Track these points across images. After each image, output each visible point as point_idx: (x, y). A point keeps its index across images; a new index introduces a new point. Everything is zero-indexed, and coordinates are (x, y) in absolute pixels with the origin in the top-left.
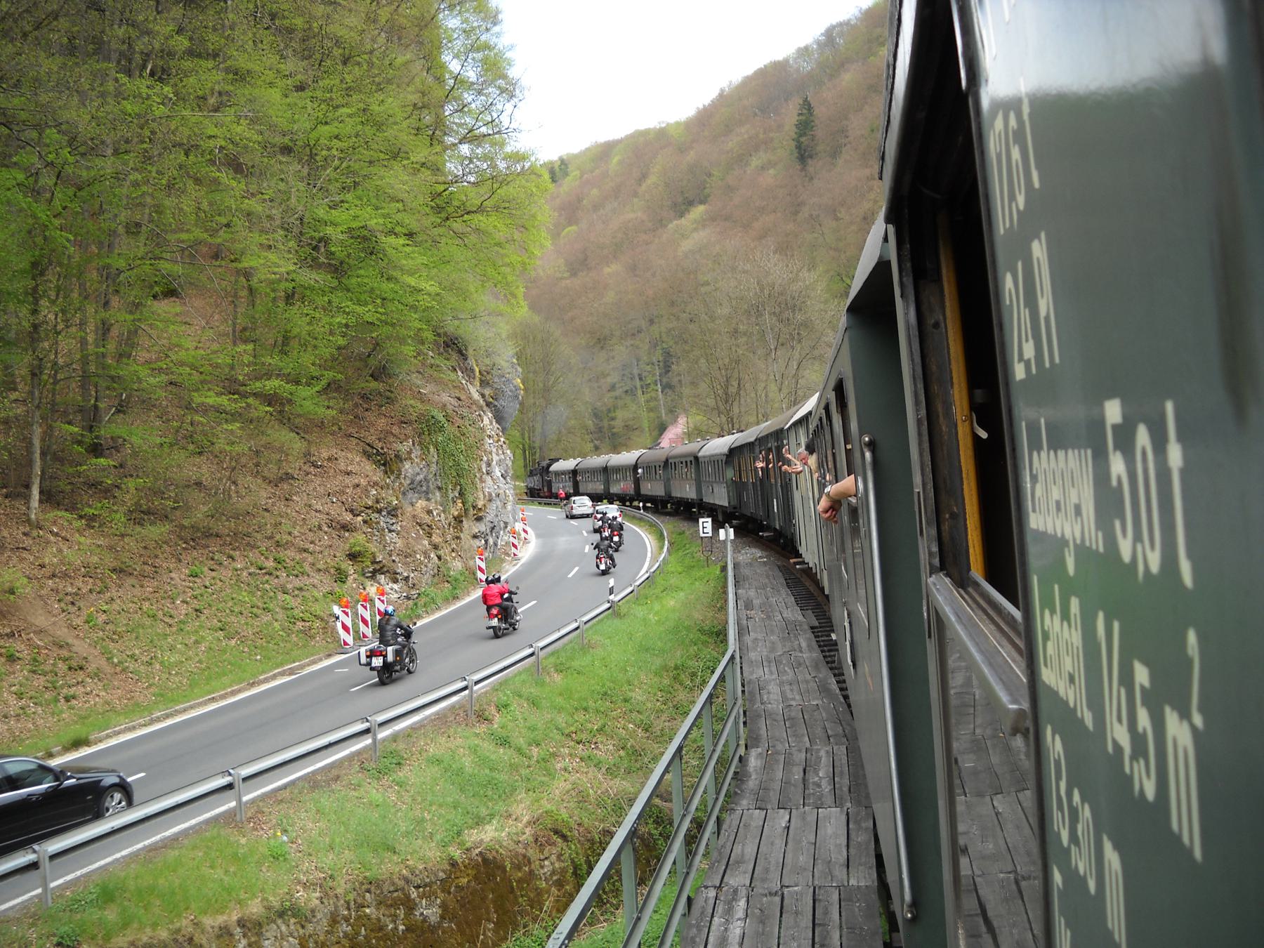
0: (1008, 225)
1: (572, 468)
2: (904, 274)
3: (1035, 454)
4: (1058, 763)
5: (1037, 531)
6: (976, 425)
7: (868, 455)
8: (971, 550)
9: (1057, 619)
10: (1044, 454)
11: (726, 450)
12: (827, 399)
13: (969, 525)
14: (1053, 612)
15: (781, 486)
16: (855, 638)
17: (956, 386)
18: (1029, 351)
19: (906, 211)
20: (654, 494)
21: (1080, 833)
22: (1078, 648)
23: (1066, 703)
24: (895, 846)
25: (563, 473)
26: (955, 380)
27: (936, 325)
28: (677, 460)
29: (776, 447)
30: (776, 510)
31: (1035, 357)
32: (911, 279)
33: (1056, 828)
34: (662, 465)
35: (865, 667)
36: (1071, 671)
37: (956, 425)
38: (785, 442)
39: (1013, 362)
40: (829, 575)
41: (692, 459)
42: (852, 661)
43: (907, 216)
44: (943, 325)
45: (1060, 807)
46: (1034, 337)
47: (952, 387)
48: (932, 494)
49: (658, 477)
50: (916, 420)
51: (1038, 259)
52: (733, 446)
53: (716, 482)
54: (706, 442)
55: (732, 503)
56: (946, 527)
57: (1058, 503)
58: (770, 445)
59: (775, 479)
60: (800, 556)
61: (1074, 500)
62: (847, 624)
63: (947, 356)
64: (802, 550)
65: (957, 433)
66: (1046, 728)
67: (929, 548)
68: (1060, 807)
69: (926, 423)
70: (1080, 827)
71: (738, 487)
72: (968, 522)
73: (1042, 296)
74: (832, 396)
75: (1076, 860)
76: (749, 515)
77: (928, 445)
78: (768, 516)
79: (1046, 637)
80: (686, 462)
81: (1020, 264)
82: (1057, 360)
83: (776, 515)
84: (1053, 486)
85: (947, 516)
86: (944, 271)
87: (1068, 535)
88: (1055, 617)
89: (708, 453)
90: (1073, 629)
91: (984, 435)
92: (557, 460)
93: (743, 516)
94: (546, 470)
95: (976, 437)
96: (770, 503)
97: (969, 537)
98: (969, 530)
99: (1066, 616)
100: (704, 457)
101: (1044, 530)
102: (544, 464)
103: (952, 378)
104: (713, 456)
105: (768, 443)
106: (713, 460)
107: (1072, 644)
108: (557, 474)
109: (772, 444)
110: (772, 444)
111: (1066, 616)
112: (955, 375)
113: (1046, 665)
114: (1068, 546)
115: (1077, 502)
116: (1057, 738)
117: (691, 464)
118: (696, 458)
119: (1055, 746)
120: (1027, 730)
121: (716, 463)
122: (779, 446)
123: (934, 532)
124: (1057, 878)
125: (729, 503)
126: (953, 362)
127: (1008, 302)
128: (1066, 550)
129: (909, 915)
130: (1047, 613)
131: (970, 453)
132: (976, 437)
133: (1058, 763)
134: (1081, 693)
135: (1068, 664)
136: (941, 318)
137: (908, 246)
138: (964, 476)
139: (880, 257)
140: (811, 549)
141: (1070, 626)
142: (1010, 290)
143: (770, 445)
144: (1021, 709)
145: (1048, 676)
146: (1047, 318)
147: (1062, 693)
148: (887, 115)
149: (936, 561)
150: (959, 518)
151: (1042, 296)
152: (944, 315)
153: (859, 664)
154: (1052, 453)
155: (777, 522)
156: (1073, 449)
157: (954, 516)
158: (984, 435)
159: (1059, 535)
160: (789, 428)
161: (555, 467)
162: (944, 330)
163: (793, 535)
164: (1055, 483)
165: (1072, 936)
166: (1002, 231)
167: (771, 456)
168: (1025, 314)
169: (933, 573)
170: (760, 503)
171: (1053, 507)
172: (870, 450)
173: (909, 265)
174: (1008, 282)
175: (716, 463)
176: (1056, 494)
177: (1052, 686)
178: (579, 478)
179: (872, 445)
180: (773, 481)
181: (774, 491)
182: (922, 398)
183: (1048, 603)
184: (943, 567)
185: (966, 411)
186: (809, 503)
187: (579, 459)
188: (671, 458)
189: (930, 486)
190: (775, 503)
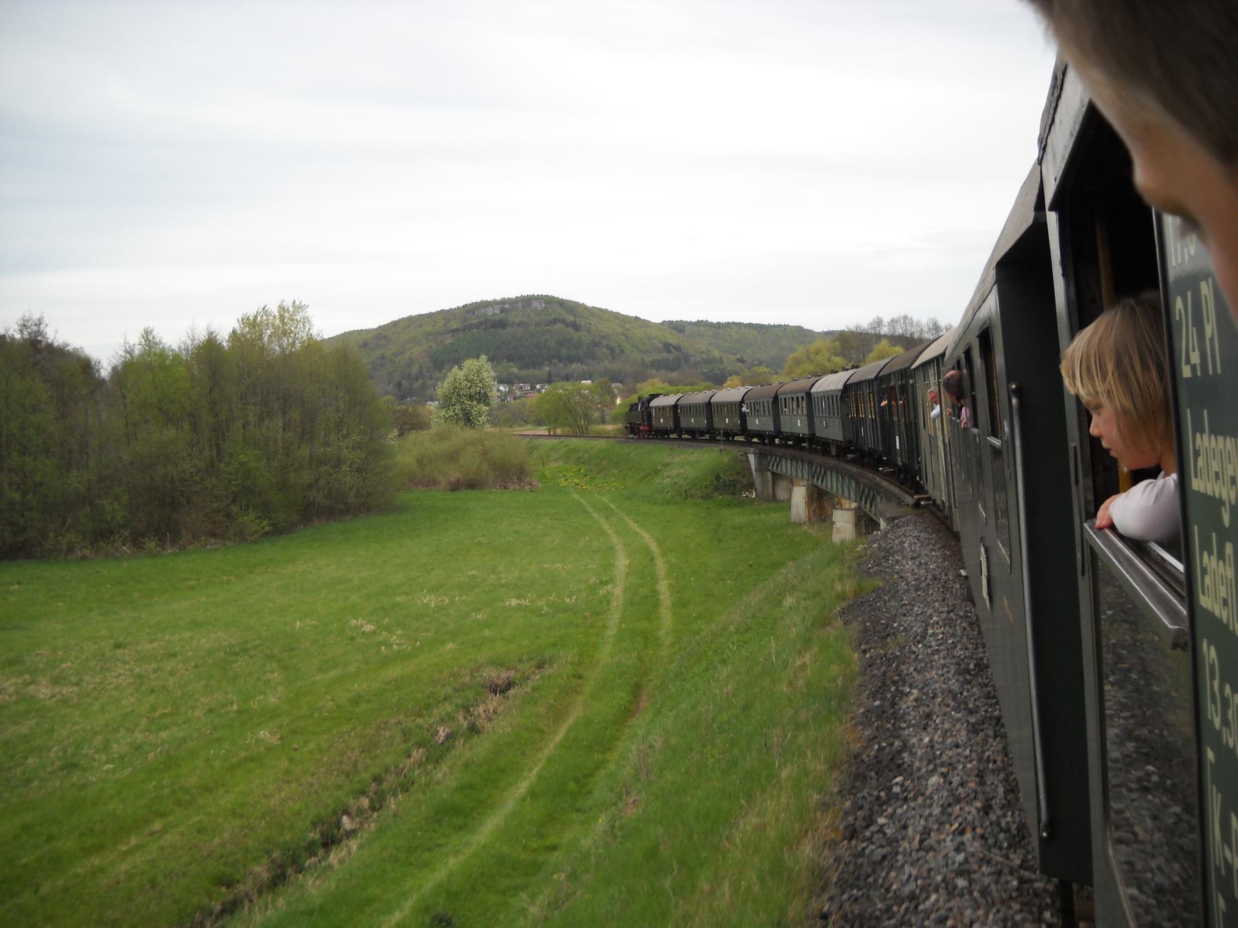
0: (1179, 262)
3: (1198, 436)
4: (1212, 667)
5: (1198, 493)
7: (1014, 401)
9: (1214, 558)
10: (1206, 436)
11: (841, 386)
14: (1210, 553)
16: (992, 574)
18: (1195, 358)
21: (1230, 717)
22: (1231, 580)
23: (1220, 621)
25: (663, 408)
28: (787, 396)
30: (898, 448)
31: (1201, 364)
33: (1210, 717)
36: (1225, 597)
39: (1180, 364)
41: (804, 395)
45: (1214, 701)
46: (1199, 349)
51: (1206, 296)
52: (849, 382)
57: (1217, 474)
60: (927, 492)
61: (1231, 473)
64: (929, 487)
66: (1203, 641)
68: (1214, 701)
70: (1230, 713)
73: (1208, 323)
75: (1227, 737)
79: (1204, 571)
80: (798, 398)
81: (1189, 293)
82: (1219, 371)
84: (1213, 462)
85: (1101, 468)
86: (1101, 254)
87: (1225, 497)
88: (1212, 557)
89: (821, 389)
90: (1227, 567)
92: (657, 396)
99: (1221, 556)
101: (1212, 495)
106: (828, 396)
107: (1226, 577)
111: (1221, 556)
113: (1204, 594)
114: (1224, 505)
115: (1233, 474)
116: (1213, 649)
118: (809, 394)
119: (1210, 654)
120: (1186, 644)
123: (1090, 482)
124: (1210, 755)
125: (844, 437)
127: (1177, 318)
128: (1223, 508)
129: (1045, 834)
130: (1205, 554)
134: (1233, 613)
135: (1223, 592)
141: (1225, 564)
142: (1180, 310)
145: (1205, 601)
146: (1212, 339)
147: (1217, 613)
148: (1051, 116)
151: (1208, 323)
152: (1100, 293)
153: (996, 598)
154: (1213, 437)
155: (899, 459)
156: (1231, 436)
159: (1217, 496)
161: (654, 403)
164: (1214, 459)
165: (1223, 799)
166: (1174, 265)
168: (1193, 331)
171: (1213, 476)
174: (1179, 304)
175: (830, 398)
176: (1215, 466)
177: (1209, 608)
179: (1019, 392)
180: (895, 419)
183: (1205, 545)
188: (781, 394)
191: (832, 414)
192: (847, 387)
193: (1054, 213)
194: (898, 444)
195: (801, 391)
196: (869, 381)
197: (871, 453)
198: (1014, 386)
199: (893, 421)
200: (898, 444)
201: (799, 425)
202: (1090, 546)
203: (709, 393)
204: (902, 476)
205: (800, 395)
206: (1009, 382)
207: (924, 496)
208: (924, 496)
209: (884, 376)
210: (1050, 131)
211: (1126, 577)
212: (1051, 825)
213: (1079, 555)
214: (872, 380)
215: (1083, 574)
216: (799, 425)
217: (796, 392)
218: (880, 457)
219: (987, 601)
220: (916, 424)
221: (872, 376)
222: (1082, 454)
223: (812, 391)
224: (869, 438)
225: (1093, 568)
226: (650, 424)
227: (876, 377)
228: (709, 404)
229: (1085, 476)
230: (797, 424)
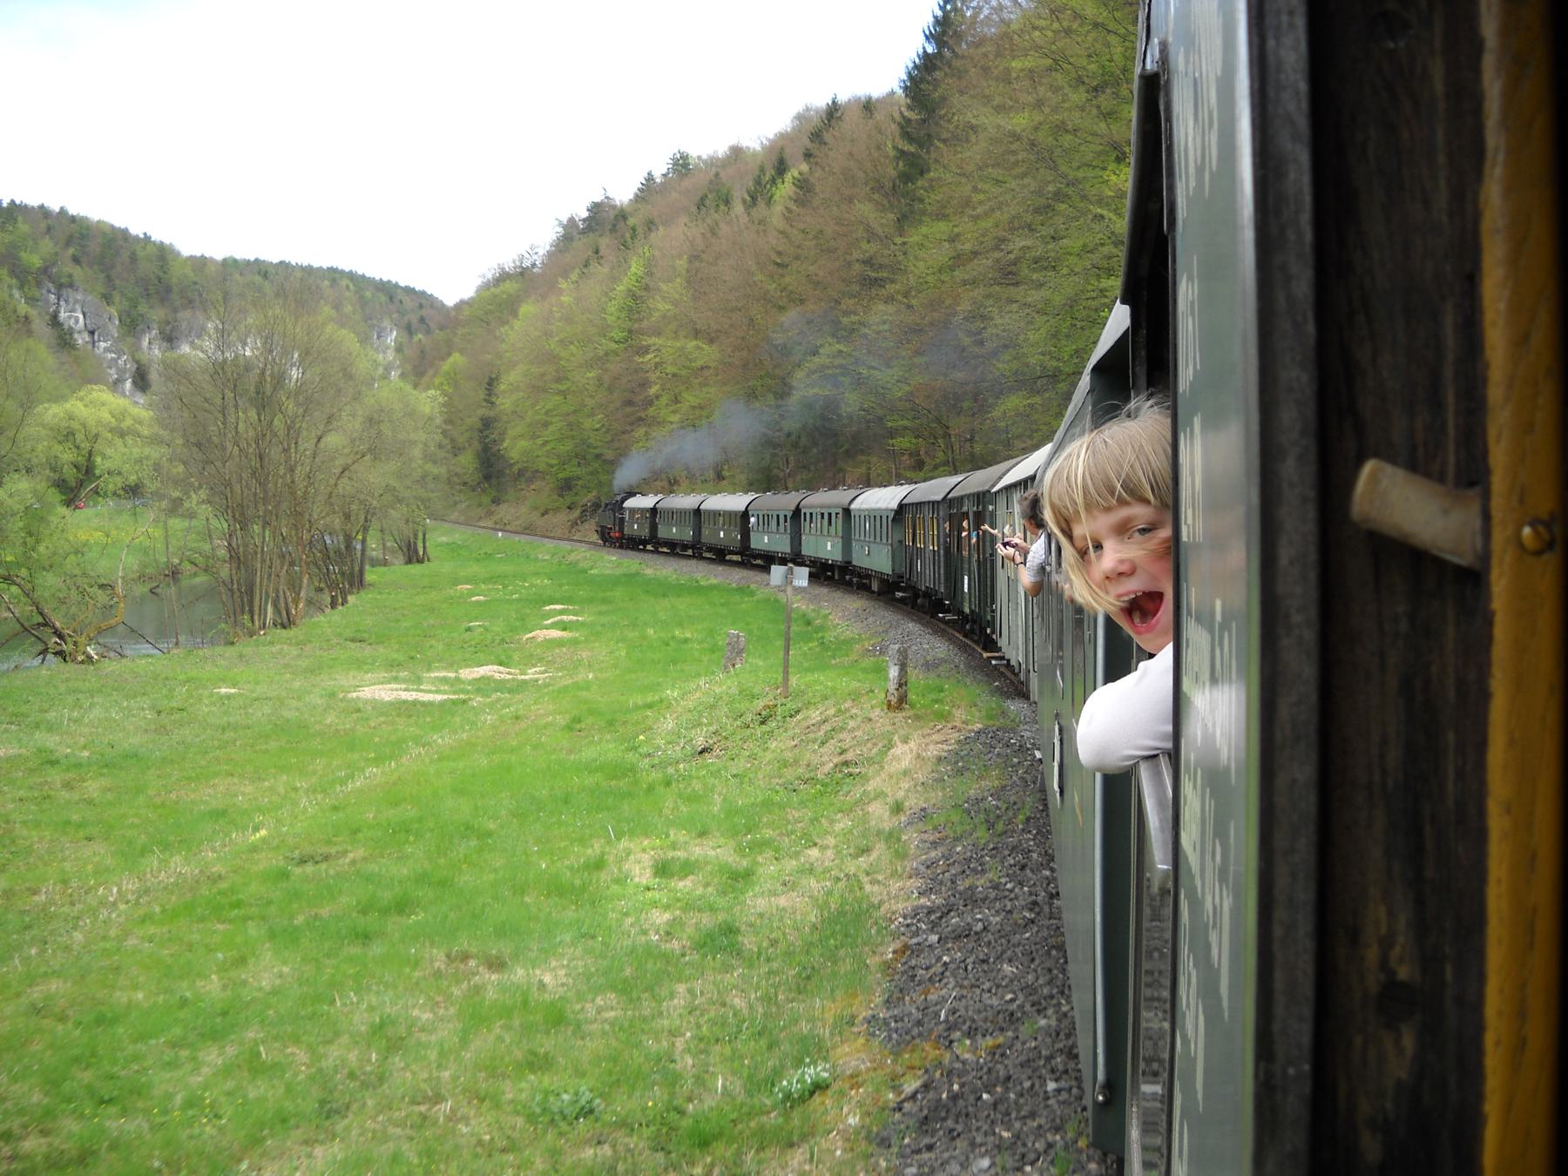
1: (652, 506)
11: (894, 505)
16: (1065, 761)
19: (1145, 293)
20: (771, 549)
29: (975, 512)
30: (966, 590)
32: (1144, 369)
34: (789, 515)
35: (1075, 797)
41: (840, 511)
42: (1059, 787)
60: (999, 650)
71: (906, 554)
80: (830, 514)
89: (865, 506)
100: (859, 510)
106: (874, 516)
108: (633, 511)
118: (847, 511)
121: (878, 519)
125: (893, 570)
129: (1101, 1098)
133: (1185, 925)
173: (1143, 353)
175: (878, 519)
180: (965, 553)
181: (966, 566)
187: (660, 496)
194: (966, 586)
200: (966, 586)
201: (829, 548)
203: (699, 498)
204: (968, 627)
207: (996, 654)
208: (996, 654)
214: (938, 502)
216: (829, 548)
218: (941, 600)
219: (1058, 795)
221: (939, 497)
224: (928, 575)
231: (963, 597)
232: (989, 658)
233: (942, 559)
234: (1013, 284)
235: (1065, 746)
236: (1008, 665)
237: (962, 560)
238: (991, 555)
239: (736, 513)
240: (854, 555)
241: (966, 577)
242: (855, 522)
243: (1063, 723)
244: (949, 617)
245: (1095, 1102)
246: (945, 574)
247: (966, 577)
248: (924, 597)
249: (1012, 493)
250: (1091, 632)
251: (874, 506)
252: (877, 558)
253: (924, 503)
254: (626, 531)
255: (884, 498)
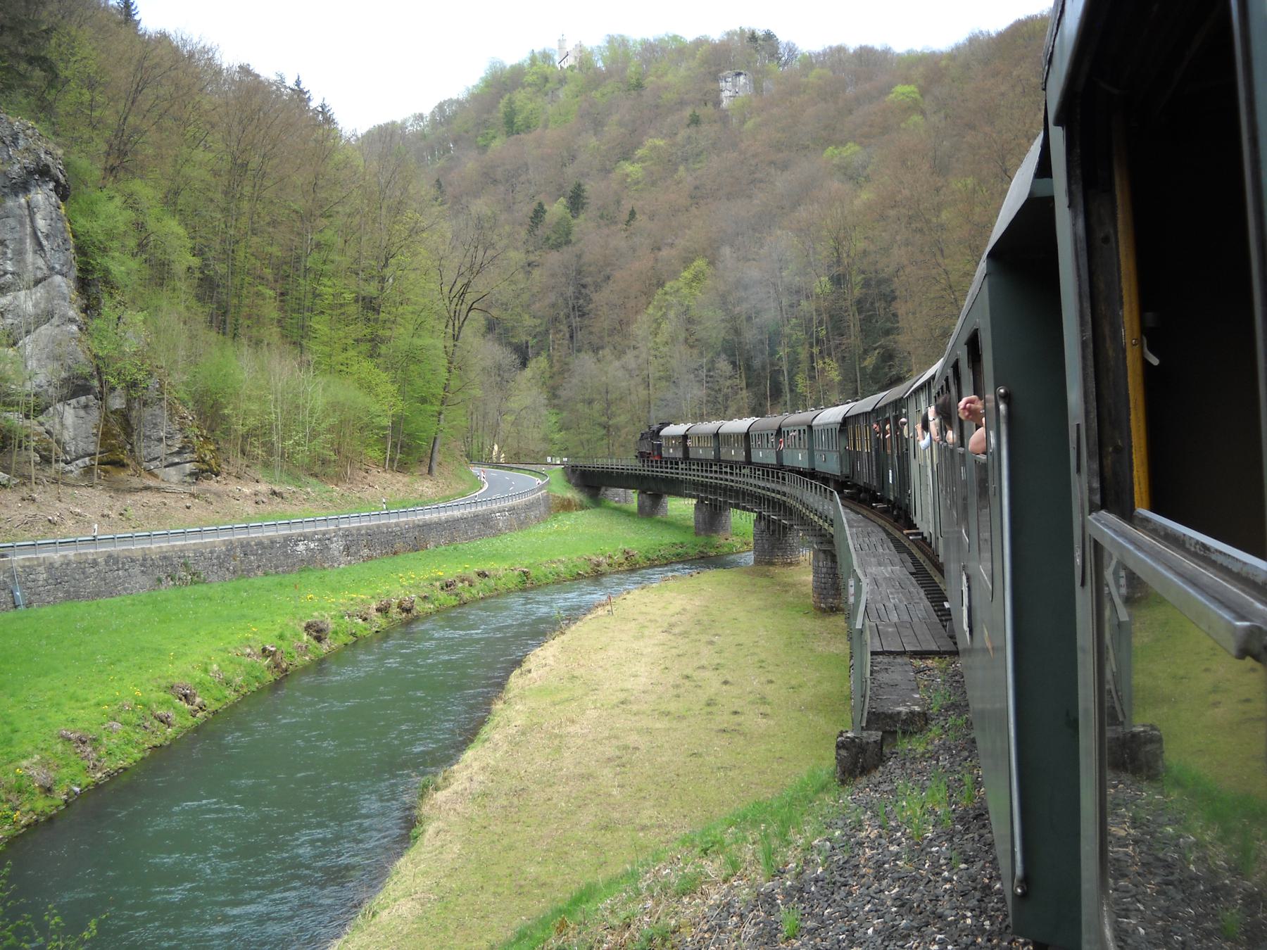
2: (1072, 182)
6: (1146, 350)
7: (1002, 407)
8: (1136, 488)
11: (840, 419)
12: (957, 355)
13: (1134, 461)
15: (898, 456)
16: (973, 604)
17: (1126, 307)
20: (764, 462)
24: (1009, 814)
25: (674, 437)
26: (1126, 299)
27: (1106, 240)
34: (775, 433)
37: (1124, 351)
38: (904, 411)
40: (947, 545)
41: (806, 427)
43: (1079, 117)
44: (1113, 239)
47: (1122, 308)
48: (1095, 425)
49: (770, 445)
50: (1080, 342)
53: (829, 451)
54: (821, 411)
55: (844, 472)
56: (1108, 461)
58: (887, 415)
59: (892, 451)
60: (914, 527)
62: (965, 590)
63: (1116, 274)
64: (917, 520)
65: (1125, 358)
67: (1089, 483)
69: (1091, 346)
71: (851, 457)
72: (1134, 456)
74: (950, 372)
76: (862, 484)
77: (1092, 369)
78: (883, 487)
80: (799, 431)
83: (891, 487)
85: (1111, 449)
89: (821, 422)
91: (1155, 361)
92: (668, 424)
93: (855, 485)
94: (656, 434)
95: (1146, 364)
96: (885, 473)
97: (1135, 472)
98: (1135, 465)
100: (818, 426)
102: (655, 427)
103: (1121, 297)
104: (827, 424)
105: (886, 413)
106: (827, 429)
108: (668, 438)
109: (890, 414)
110: (890, 414)
112: (1125, 293)
117: (804, 433)
118: (810, 427)
122: (897, 416)
123: (1095, 466)
125: (842, 472)
126: (1123, 280)
129: (1019, 890)
131: (1139, 379)
132: (1146, 364)
136: (1112, 231)
137: (1079, 151)
138: (1132, 405)
139: (1031, 193)
140: (925, 520)
143: (887, 415)
144: (1253, 626)
149: (1097, 498)
150: (1123, 452)
155: (892, 493)
157: (1118, 450)
158: (1155, 361)
160: (909, 396)
161: (666, 431)
162: (1114, 245)
163: (908, 506)
167: (888, 427)
169: (1093, 511)
170: (875, 474)
172: (1005, 402)
173: (1078, 172)
178: (689, 443)
179: (1007, 398)
180: (889, 451)
181: (890, 462)
182: (1089, 318)
184: (1104, 505)
185: (1137, 334)
186: (926, 471)
187: (690, 425)
189: (1093, 415)
190: (890, 474)
191: (831, 447)
192: (846, 420)
193: (1060, 128)
194: (891, 478)
195: (802, 424)
196: (866, 413)
197: (866, 489)
198: (1002, 391)
199: (887, 455)
200: (891, 478)
201: (800, 458)
202: (1096, 542)
203: (718, 423)
204: (895, 513)
205: (802, 428)
206: (996, 386)
207: (914, 531)
208: (914, 531)
209: (880, 408)
210: (1057, 29)
211: (1166, 578)
212: (1026, 880)
213: (1078, 561)
214: (869, 412)
215: (1083, 584)
216: (800, 458)
217: (799, 425)
218: (875, 492)
219: (968, 634)
220: (907, 455)
221: (869, 409)
222: (1087, 430)
223: (814, 423)
224: (865, 475)
225: (1097, 582)
226: (660, 455)
227: (873, 409)
228: (717, 435)
229: (1090, 456)
230: (799, 459)
231: (888, 488)
232: (908, 534)
233: (874, 459)
234: (431, 461)
235: (973, 591)
236: (924, 539)
237: (887, 458)
238: (907, 450)
239: (738, 435)
240: (816, 463)
241: (890, 471)
242: (816, 435)
243: (969, 573)
244: (880, 506)
245: (1015, 895)
246: (876, 468)
247: (890, 471)
248: (865, 492)
249: (919, 395)
250: (996, 485)
251: (827, 421)
252: (831, 464)
253: (860, 414)
254: (664, 454)
255: (833, 415)
